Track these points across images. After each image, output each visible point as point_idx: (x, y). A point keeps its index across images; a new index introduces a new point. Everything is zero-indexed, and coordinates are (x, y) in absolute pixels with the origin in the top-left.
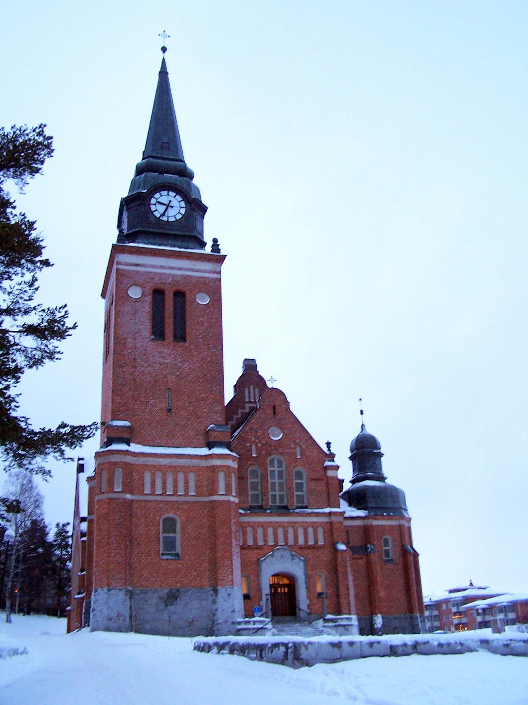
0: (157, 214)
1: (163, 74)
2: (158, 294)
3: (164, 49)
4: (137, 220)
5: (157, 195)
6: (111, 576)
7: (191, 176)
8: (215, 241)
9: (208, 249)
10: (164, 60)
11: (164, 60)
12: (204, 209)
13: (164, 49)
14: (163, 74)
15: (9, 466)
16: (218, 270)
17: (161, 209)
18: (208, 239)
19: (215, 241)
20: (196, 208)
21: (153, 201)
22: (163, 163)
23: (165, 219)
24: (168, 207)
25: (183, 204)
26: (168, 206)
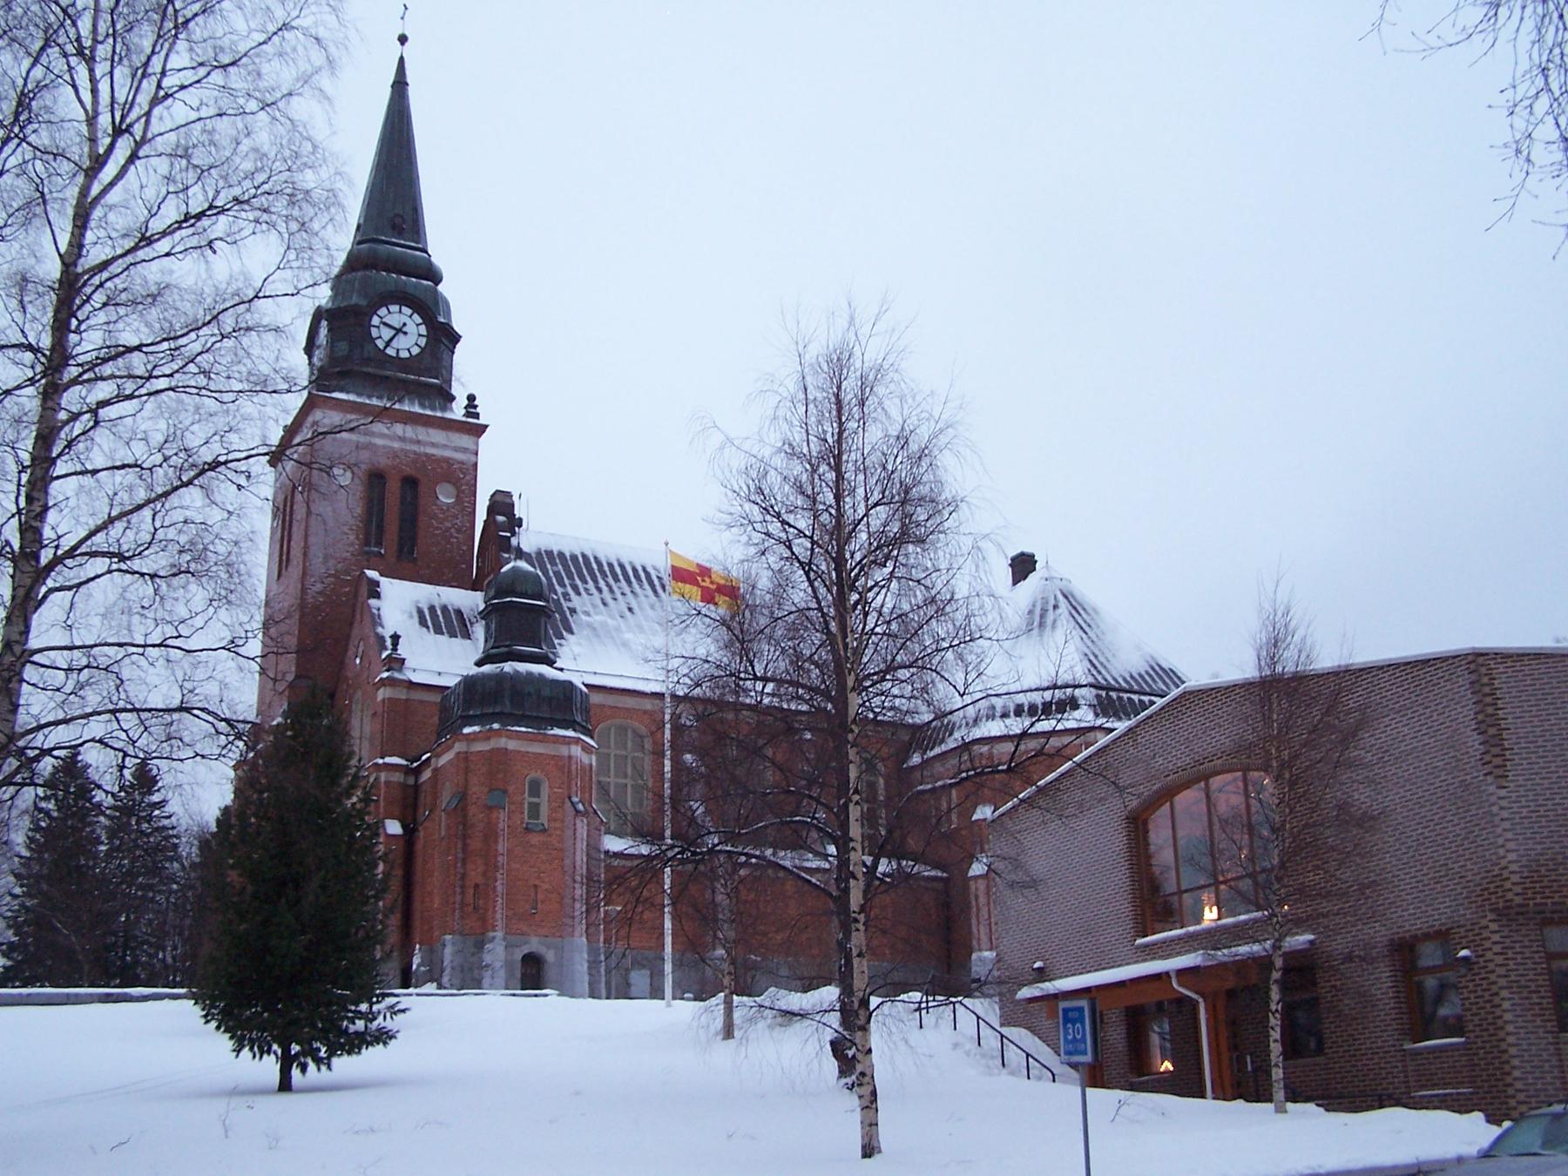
0: (380, 344)
1: (400, 85)
2: (376, 479)
3: (403, 39)
4: (344, 347)
5: (383, 311)
6: (162, 383)
7: (436, 277)
8: (471, 398)
9: (458, 411)
10: (402, 60)
11: (402, 60)
12: (455, 338)
13: (403, 39)
14: (400, 85)
15: (1560, 45)
16: (472, 447)
17: (387, 334)
18: (460, 393)
19: (471, 398)
20: (443, 337)
21: (375, 321)
22: (390, 259)
23: (390, 352)
24: (398, 331)
25: (423, 330)
26: (399, 331)
